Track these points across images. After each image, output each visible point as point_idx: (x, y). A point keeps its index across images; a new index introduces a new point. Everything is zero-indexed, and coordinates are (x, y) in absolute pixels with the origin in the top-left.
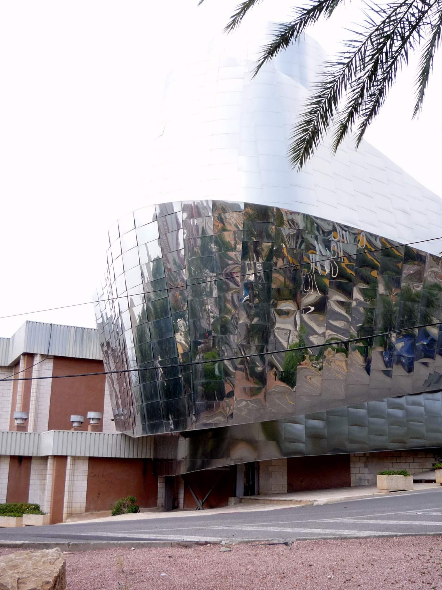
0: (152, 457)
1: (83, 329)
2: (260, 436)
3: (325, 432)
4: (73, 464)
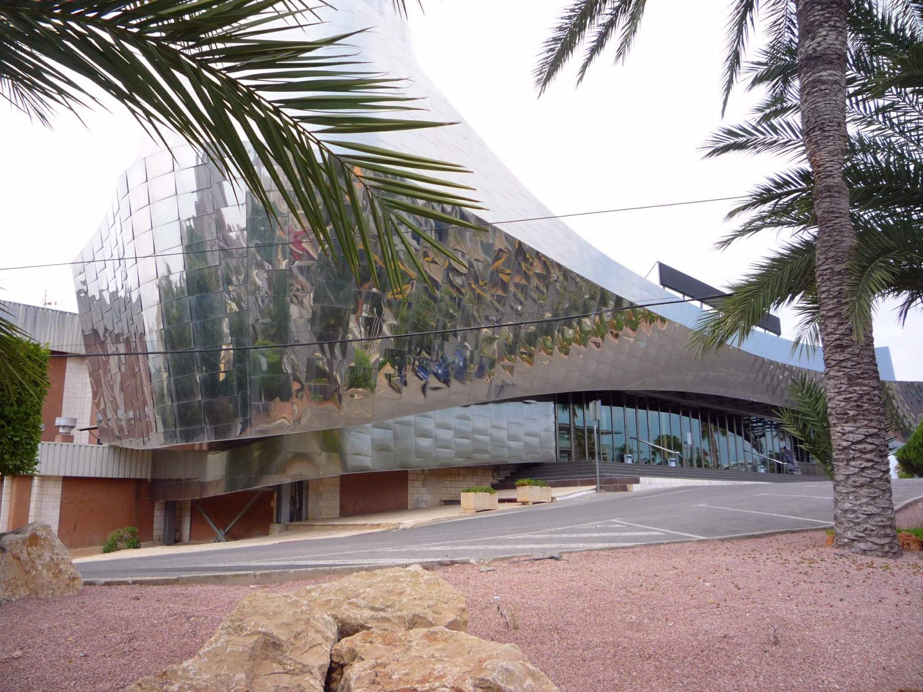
0: (149, 477)
1: (36, 309)
2: (313, 447)
3: (392, 444)
4: (41, 487)
